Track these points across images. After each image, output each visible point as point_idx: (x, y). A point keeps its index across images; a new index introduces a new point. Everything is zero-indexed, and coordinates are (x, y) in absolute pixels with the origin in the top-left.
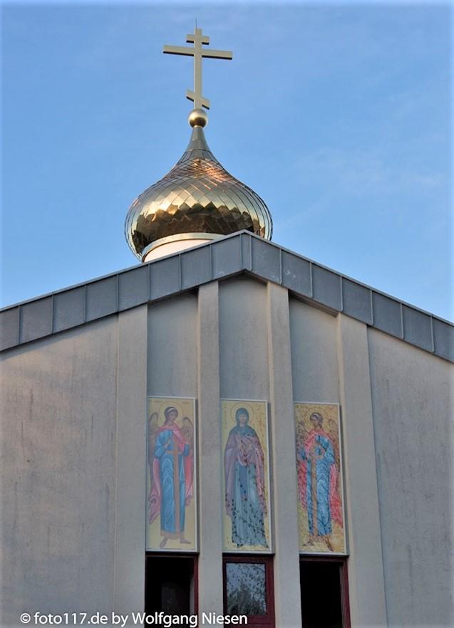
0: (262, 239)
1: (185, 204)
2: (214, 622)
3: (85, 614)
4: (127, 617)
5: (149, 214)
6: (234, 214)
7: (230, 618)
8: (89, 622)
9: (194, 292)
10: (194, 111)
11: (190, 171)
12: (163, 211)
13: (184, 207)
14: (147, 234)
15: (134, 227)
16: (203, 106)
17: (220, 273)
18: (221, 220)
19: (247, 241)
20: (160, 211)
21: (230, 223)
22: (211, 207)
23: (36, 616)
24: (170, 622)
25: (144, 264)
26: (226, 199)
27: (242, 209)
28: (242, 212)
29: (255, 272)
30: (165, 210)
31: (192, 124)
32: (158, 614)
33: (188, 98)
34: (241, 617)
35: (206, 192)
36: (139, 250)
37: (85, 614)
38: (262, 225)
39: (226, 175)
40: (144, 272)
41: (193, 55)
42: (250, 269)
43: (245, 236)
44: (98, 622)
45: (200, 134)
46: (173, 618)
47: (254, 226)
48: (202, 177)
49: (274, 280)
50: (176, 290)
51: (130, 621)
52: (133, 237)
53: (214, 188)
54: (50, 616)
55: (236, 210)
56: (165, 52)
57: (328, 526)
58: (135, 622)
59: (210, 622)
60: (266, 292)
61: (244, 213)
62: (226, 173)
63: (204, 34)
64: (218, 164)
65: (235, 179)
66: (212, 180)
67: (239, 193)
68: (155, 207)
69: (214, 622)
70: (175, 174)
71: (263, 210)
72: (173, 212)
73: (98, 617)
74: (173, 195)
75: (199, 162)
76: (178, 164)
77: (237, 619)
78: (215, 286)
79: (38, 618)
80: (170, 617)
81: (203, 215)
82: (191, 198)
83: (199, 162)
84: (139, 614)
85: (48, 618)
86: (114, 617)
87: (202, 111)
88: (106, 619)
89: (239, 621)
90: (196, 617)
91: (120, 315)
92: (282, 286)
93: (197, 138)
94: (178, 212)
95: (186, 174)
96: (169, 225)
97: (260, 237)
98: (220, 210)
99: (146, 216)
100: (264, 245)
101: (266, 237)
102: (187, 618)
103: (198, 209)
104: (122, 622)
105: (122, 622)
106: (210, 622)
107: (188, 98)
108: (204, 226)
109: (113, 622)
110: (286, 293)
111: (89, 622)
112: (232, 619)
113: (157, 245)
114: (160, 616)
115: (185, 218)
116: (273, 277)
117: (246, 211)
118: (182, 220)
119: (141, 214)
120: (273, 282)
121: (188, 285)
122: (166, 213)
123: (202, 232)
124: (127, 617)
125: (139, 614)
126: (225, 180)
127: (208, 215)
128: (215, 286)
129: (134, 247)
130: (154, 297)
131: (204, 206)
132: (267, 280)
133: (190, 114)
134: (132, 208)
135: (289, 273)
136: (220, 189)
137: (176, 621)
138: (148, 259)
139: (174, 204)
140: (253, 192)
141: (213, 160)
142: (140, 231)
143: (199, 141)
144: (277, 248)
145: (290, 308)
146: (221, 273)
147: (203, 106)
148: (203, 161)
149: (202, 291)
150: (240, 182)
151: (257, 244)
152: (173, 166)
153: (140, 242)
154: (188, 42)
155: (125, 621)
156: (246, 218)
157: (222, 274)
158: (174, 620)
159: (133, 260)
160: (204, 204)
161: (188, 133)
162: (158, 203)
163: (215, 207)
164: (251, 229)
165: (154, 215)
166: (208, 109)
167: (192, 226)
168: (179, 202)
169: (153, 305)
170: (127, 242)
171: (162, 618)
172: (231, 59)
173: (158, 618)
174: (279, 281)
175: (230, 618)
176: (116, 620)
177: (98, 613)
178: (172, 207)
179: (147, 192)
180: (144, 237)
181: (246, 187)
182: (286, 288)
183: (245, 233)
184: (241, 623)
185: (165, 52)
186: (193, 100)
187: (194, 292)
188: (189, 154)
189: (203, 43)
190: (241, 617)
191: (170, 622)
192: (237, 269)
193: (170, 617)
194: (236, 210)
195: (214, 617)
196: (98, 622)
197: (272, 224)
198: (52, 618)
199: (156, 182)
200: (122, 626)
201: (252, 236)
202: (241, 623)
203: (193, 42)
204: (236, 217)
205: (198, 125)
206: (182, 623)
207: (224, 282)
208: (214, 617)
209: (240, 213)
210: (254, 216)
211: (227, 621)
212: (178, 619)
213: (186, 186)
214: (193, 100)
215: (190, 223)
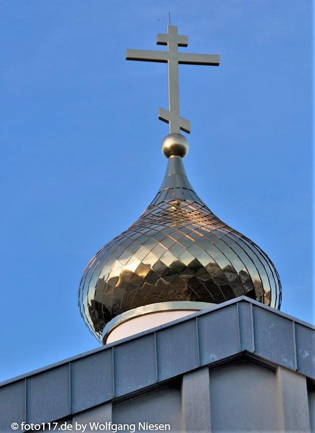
0: (268, 308)
1: (160, 263)
2: (147, 429)
3: (57, 423)
4: (86, 425)
5: (111, 276)
6: (228, 275)
7: (158, 426)
8: (59, 429)
9: (174, 385)
10: (170, 136)
11: (166, 216)
12: (131, 272)
13: (160, 266)
14: (109, 305)
15: (91, 296)
16: (182, 129)
17: (211, 356)
18: (210, 283)
19: (247, 310)
20: (126, 272)
21: (222, 287)
22: (196, 266)
23: (22, 425)
24: (116, 429)
25: (105, 347)
26: (215, 254)
27: (239, 267)
28: (238, 271)
29: (260, 354)
30: (134, 272)
31: (168, 153)
32: (108, 424)
33: (160, 118)
34: (166, 425)
35: (189, 246)
36: (99, 327)
37: (57, 423)
38: (267, 289)
39: (215, 221)
40: (108, 357)
41: (166, 62)
42: (252, 350)
43: (243, 305)
44: (65, 429)
45: (179, 167)
46: (118, 426)
47: (256, 290)
48: (183, 224)
49: (287, 366)
50: (151, 381)
51: (88, 428)
52: (90, 309)
53: (199, 241)
54: (32, 425)
55: (230, 269)
56: (128, 59)
57: (164, 203)
58: (92, 429)
59: (144, 429)
60: (236, 306)
61: (242, 272)
62: (215, 218)
63: (179, 33)
64: (204, 206)
65: (227, 227)
66: (197, 229)
67: (234, 246)
68: (117, 269)
69: (147, 429)
70: (144, 221)
71: (267, 268)
72: (144, 274)
73: (65, 425)
74: (144, 251)
75: (178, 204)
76: (149, 208)
77: (163, 427)
78: (205, 375)
79: (24, 426)
80: (116, 425)
81: (184, 277)
82: (168, 253)
83: (178, 204)
84: (94, 423)
85: (31, 426)
86: (77, 425)
87: (179, 136)
88: (72, 427)
89: (164, 428)
90: (134, 425)
91: (74, 419)
92: (297, 372)
93: (174, 173)
94: (151, 273)
95: (160, 221)
96: (139, 291)
97: (265, 306)
98: (209, 269)
99: (107, 280)
100: (271, 317)
101: (273, 305)
102: (128, 426)
103: (178, 268)
104: (82, 429)
105: (82, 429)
106: (144, 429)
107: (160, 118)
108: (188, 292)
109: (76, 429)
110: (303, 383)
111: (59, 429)
112: (160, 427)
113: (123, 320)
114: (109, 425)
115: (161, 282)
116: (285, 361)
117: (245, 270)
118: (156, 284)
119: (101, 277)
120: (284, 368)
121: (167, 374)
122: (134, 275)
123: (185, 300)
124: (86, 425)
125: (94, 423)
126: (214, 228)
127: (191, 276)
128: (205, 375)
129: (92, 323)
130: (123, 391)
131: (187, 265)
132: (277, 365)
133: (164, 140)
134: (88, 270)
135: (307, 354)
136: (206, 241)
137: (120, 428)
138: (112, 339)
139: (145, 262)
140: (253, 244)
141: (197, 201)
142: (100, 301)
143: (177, 176)
144: (289, 320)
145: (308, 396)
146: (212, 357)
147: (182, 129)
148: (183, 203)
149: (186, 383)
150: (234, 231)
151: (261, 316)
152: (143, 210)
153: (100, 317)
154: (159, 43)
155: (84, 429)
156: (244, 279)
157: (213, 358)
158: (119, 427)
159: (93, 343)
160: (187, 262)
161: (163, 166)
162: (124, 262)
163: (202, 266)
164: (252, 295)
165: (117, 278)
166: (188, 132)
167: (171, 292)
168: (152, 261)
169: (120, 404)
170: (79, 305)
171: (111, 426)
172: (217, 65)
173: (108, 426)
174: (293, 365)
175: (158, 426)
176: (78, 427)
177: (66, 423)
178: (142, 266)
179: (108, 247)
180: (106, 310)
181: (243, 237)
182: (304, 376)
183: (243, 301)
184: (166, 429)
185: (128, 59)
186: (167, 122)
187: (174, 385)
188: (164, 194)
189: (180, 45)
190: (166, 425)
191: (116, 429)
192: (233, 351)
193: (116, 425)
194: (230, 269)
195: (147, 425)
196: (65, 429)
197: (280, 287)
198: (34, 426)
199: (119, 234)
200: (83, 431)
201: (253, 305)
202: (166, 429)
203: (165, 44)
204: (230, 278)
205: (175, 154)
206: (124, 429)
207: (216, 368)
208: (147, 425)
209: (236, 272)
210: (255, 277)
211: (156, 428)
212: (122, 427)
213: (160, 237)
214: (167, 122)
215: (168, 288)
